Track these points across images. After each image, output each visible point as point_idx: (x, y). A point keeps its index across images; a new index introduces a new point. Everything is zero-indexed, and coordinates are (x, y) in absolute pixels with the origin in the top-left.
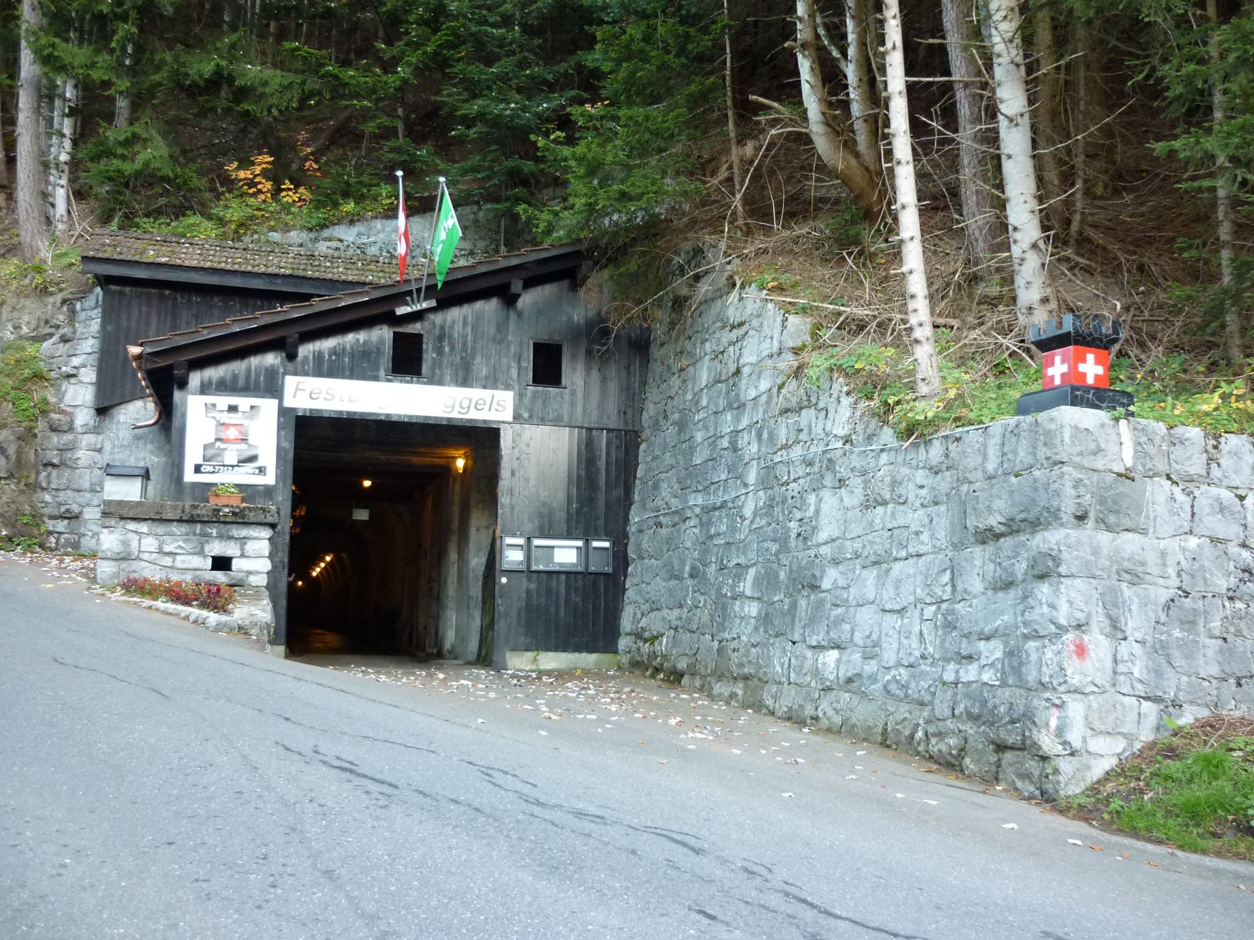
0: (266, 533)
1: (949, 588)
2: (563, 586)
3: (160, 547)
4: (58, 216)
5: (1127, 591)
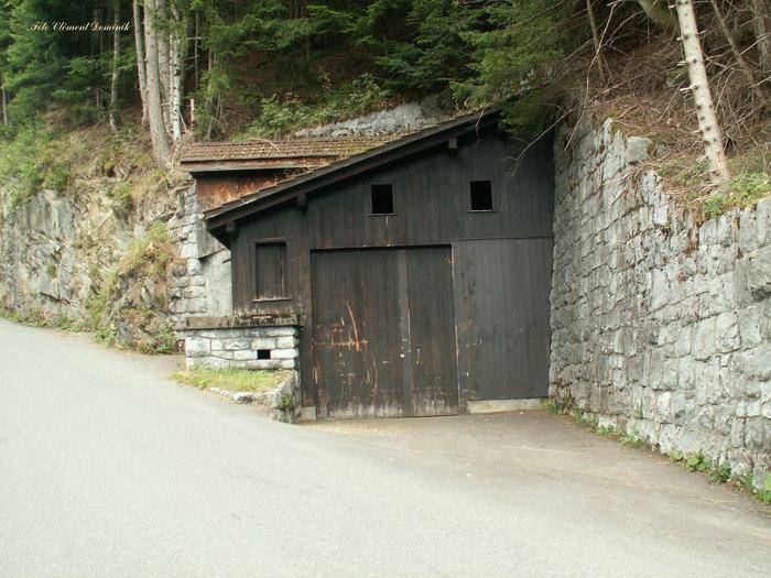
0: (291, 332)
1: (737, 339)
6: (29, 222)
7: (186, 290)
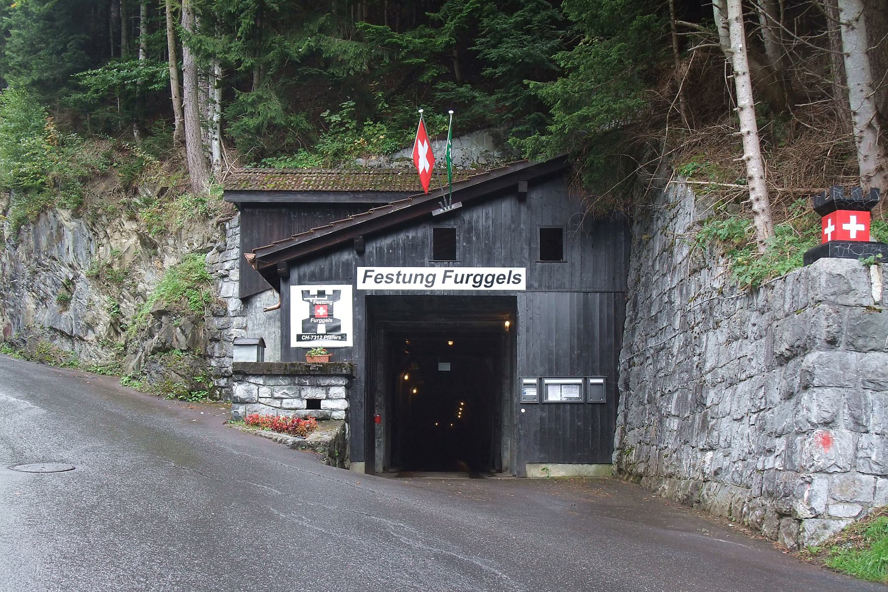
1: (763, 400)
2: (568, 414)
3: (272, 395)
4: (214, 161)
5: (870, 396)
6: (37, 244)
7: (225, 332)
